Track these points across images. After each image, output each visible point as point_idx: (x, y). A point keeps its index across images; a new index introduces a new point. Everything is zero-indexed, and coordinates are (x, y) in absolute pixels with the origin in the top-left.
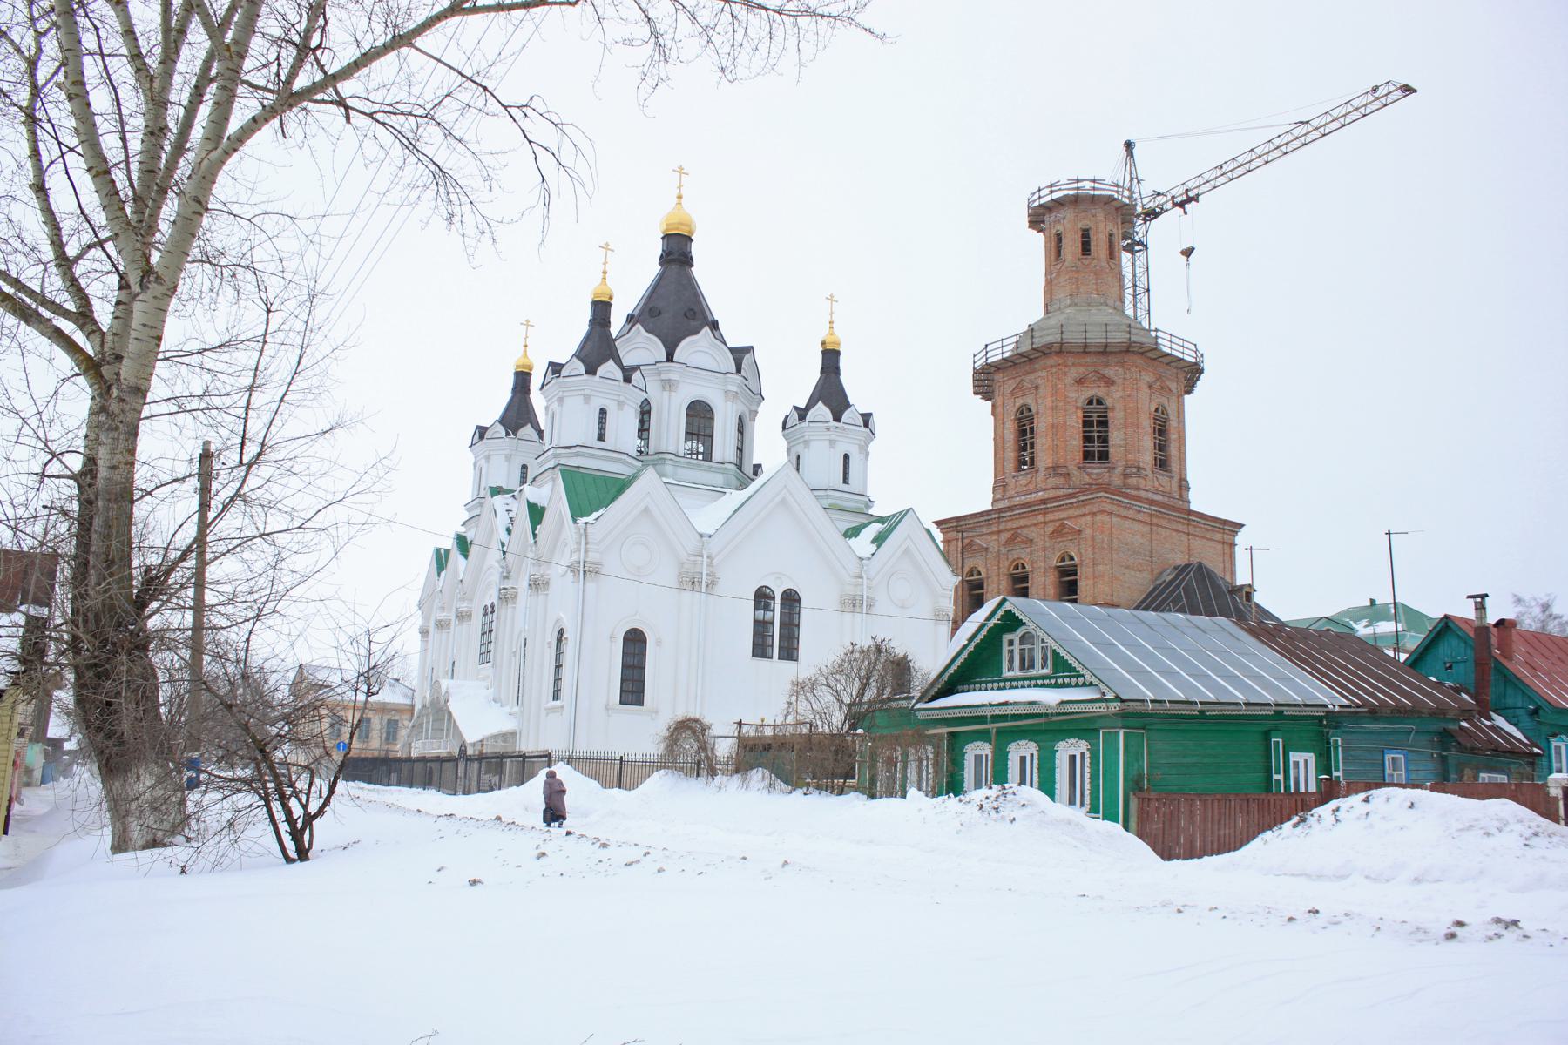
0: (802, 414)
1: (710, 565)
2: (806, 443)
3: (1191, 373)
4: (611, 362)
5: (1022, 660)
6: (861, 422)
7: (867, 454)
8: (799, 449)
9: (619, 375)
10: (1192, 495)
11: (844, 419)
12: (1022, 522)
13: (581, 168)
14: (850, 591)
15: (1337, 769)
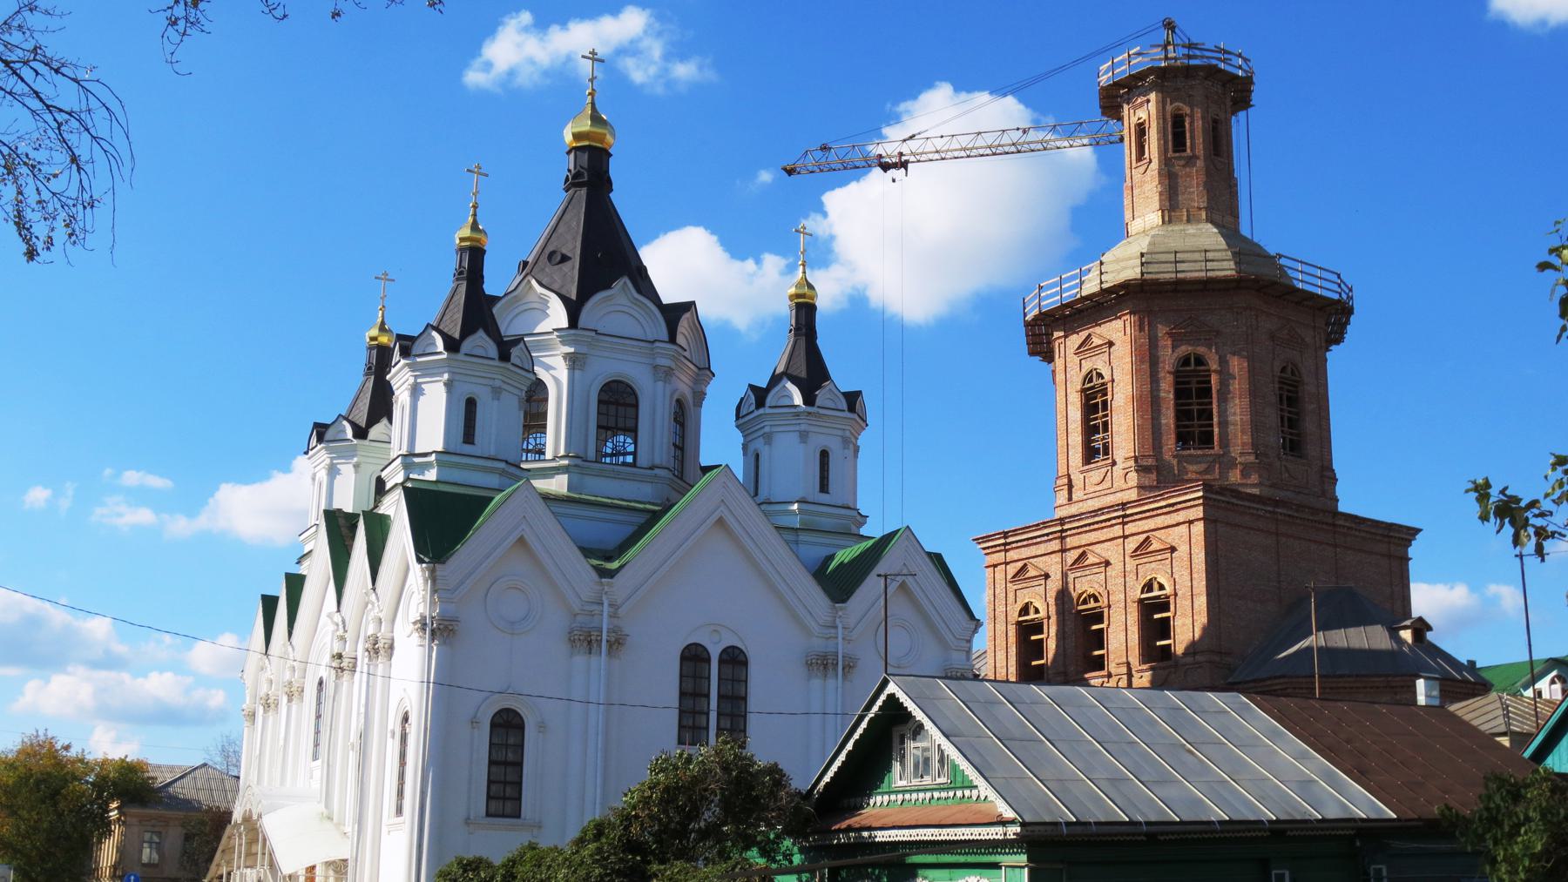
1: (613, 616)
2: (768, 438)
3: (1331, 317)
4: (481, 333)
5: (916, 766)
6: (844, 406)
7: (857, 449)
8: (759, 444)
9: (493, 351)
10: (1341, 490)
11: (818, 402)
12: (1093, 537)
14: (818, 645)
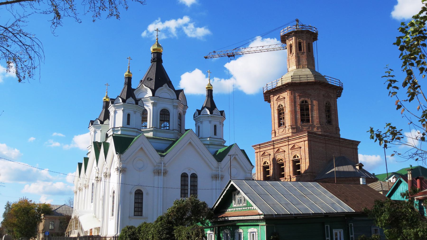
0: (199, 112)
1: (164, 166)
2: (201, 122)
3: (338, 91)
6: (220, 114)
7: (223, 125)
9: (134, 102)
10: (341, 133)
13: (42, 54)
15: (352, 234)
